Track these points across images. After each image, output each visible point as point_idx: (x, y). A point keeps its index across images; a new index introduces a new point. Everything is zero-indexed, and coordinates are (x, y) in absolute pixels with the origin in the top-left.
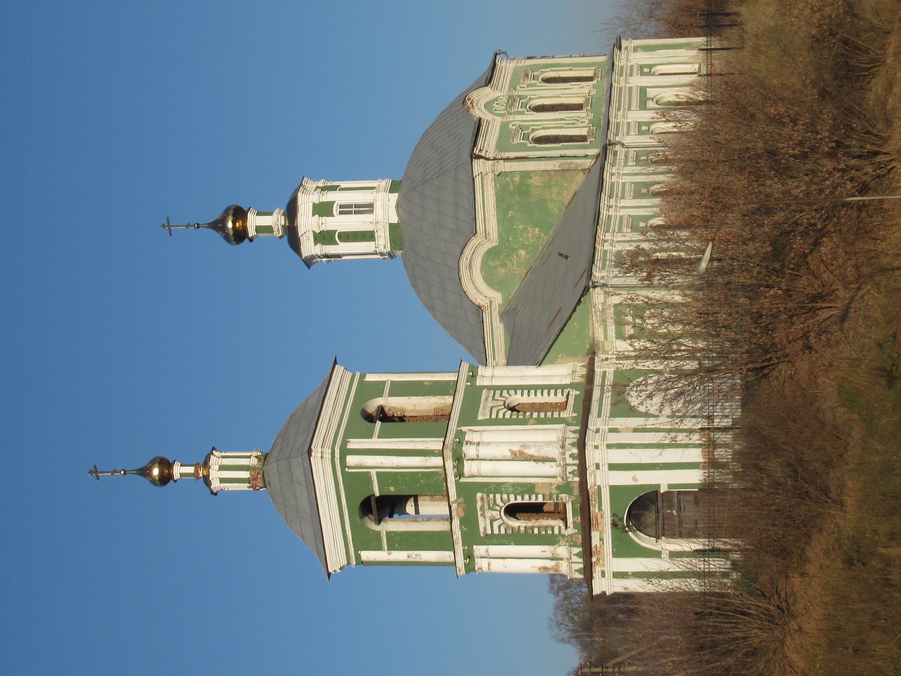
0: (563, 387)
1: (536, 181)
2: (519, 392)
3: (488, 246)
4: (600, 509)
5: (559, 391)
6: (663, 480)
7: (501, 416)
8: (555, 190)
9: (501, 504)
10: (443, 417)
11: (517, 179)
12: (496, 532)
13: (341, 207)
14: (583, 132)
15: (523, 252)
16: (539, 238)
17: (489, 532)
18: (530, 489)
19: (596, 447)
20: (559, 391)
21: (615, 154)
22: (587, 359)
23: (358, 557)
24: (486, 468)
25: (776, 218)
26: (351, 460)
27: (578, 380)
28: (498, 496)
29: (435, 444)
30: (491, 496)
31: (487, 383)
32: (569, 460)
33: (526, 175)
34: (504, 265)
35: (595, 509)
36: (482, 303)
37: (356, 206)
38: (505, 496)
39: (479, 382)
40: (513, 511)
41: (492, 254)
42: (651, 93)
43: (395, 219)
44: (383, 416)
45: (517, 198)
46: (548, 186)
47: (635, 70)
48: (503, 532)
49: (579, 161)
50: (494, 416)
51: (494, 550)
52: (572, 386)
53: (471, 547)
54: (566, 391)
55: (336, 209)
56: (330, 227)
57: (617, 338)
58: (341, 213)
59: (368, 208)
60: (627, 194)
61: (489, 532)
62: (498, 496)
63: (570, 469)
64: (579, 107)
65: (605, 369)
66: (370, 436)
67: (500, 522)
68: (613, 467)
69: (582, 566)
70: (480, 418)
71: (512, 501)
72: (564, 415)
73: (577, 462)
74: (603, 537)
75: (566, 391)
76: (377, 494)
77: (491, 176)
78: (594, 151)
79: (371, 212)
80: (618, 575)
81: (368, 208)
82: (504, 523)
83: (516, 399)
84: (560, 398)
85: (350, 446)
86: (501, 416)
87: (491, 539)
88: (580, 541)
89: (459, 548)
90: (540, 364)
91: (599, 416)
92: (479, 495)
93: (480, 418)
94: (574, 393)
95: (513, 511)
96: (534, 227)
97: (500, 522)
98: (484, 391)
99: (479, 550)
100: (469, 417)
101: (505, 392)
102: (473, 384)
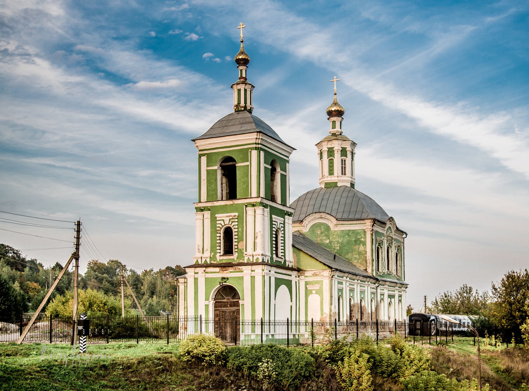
0: (284, 256)
1: (362, 248)
2: (283, 235)
3: (331, 225)
4: (231, 272)
5: (283, 254)
6: (245, 302)
7: (274, 226)
8: (357, 256)
9: (232, 225)
10: (273, 199)
11: (363, 239)
12: (218, 222)
13: (345, 160)
14: (380, 270)
15: (328, 241)
16: (334, 249)
17: (217, 219)
18: (240, 239)
19: (263, 270)
20: (283, 254)
21: (375, 284)
22: (296, 268)
23: (204, 155)
24: (250, 219)
25: (46, 357)
26: (254, 153)
27: (287, 263)
28: (236, 223)
29: (262, 194)
30: (236, 220)
31: (286, 221)
32: (255, 258)
33: (364, 244)
34: (322, 233)
35: (231, 270)
36: (304, 223)
37: (345, 167)
38: (236, 227)
39: (286, 217)
40: (228, 232)
41: (328, 228)
42: (393, 300)
43: (339, 184)
44: (273, 171)
45: (354, 239)
46: (360, 253)
47: (400, 293)
48: (218, 225)
49: (371, 267)
50: (274, 223)
51: (208, 222)
52: (285, 261)
53: (209, 210)
54: (283, 257)
55: (344, 158)
56: (336, 155)
57: (306, 282)
58: (342, 160)
59: (344, 173)
60: (362, 288)
61: (217, 219)
62: (236, 223)
63: (251, 258)
64: (388, 269)
65: (293, 277)
66: (265, 162)
67: (223, 224)
68: (253, 278)
69: (200, 263)
70: (273, 216)
71: (234, 230)
72: (274, 256)
73: (255, 261)
74: (217, 274)
75: (283, 257)
76: (237, 165)
77: (364, 228)
78: (374, 275)
79: (342, 174)
80: (196, 280)
81: (344, 173)
82: (223, 226)
83: (280, 235)
84: (280, 254)
85: (262, 152)
86: (274, 226)
87: (213, 220)
88: (213, 262)
89: (209, 204)
90: (293, 246)
91: (275, 272)
92: (237, 214)
93: (273, 216)
94: (283, 261)
95: (228, 232)
96: (340, 247)
97: (223, 224)
98: (283, 219)
99: (207, 214)
100: (274, 211)
101: (282, 229)
102: (286, 214)
